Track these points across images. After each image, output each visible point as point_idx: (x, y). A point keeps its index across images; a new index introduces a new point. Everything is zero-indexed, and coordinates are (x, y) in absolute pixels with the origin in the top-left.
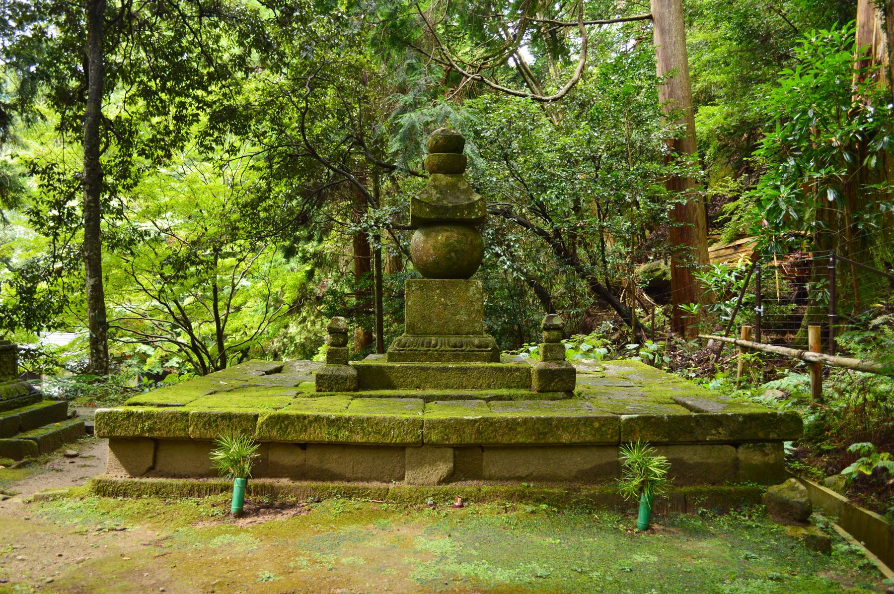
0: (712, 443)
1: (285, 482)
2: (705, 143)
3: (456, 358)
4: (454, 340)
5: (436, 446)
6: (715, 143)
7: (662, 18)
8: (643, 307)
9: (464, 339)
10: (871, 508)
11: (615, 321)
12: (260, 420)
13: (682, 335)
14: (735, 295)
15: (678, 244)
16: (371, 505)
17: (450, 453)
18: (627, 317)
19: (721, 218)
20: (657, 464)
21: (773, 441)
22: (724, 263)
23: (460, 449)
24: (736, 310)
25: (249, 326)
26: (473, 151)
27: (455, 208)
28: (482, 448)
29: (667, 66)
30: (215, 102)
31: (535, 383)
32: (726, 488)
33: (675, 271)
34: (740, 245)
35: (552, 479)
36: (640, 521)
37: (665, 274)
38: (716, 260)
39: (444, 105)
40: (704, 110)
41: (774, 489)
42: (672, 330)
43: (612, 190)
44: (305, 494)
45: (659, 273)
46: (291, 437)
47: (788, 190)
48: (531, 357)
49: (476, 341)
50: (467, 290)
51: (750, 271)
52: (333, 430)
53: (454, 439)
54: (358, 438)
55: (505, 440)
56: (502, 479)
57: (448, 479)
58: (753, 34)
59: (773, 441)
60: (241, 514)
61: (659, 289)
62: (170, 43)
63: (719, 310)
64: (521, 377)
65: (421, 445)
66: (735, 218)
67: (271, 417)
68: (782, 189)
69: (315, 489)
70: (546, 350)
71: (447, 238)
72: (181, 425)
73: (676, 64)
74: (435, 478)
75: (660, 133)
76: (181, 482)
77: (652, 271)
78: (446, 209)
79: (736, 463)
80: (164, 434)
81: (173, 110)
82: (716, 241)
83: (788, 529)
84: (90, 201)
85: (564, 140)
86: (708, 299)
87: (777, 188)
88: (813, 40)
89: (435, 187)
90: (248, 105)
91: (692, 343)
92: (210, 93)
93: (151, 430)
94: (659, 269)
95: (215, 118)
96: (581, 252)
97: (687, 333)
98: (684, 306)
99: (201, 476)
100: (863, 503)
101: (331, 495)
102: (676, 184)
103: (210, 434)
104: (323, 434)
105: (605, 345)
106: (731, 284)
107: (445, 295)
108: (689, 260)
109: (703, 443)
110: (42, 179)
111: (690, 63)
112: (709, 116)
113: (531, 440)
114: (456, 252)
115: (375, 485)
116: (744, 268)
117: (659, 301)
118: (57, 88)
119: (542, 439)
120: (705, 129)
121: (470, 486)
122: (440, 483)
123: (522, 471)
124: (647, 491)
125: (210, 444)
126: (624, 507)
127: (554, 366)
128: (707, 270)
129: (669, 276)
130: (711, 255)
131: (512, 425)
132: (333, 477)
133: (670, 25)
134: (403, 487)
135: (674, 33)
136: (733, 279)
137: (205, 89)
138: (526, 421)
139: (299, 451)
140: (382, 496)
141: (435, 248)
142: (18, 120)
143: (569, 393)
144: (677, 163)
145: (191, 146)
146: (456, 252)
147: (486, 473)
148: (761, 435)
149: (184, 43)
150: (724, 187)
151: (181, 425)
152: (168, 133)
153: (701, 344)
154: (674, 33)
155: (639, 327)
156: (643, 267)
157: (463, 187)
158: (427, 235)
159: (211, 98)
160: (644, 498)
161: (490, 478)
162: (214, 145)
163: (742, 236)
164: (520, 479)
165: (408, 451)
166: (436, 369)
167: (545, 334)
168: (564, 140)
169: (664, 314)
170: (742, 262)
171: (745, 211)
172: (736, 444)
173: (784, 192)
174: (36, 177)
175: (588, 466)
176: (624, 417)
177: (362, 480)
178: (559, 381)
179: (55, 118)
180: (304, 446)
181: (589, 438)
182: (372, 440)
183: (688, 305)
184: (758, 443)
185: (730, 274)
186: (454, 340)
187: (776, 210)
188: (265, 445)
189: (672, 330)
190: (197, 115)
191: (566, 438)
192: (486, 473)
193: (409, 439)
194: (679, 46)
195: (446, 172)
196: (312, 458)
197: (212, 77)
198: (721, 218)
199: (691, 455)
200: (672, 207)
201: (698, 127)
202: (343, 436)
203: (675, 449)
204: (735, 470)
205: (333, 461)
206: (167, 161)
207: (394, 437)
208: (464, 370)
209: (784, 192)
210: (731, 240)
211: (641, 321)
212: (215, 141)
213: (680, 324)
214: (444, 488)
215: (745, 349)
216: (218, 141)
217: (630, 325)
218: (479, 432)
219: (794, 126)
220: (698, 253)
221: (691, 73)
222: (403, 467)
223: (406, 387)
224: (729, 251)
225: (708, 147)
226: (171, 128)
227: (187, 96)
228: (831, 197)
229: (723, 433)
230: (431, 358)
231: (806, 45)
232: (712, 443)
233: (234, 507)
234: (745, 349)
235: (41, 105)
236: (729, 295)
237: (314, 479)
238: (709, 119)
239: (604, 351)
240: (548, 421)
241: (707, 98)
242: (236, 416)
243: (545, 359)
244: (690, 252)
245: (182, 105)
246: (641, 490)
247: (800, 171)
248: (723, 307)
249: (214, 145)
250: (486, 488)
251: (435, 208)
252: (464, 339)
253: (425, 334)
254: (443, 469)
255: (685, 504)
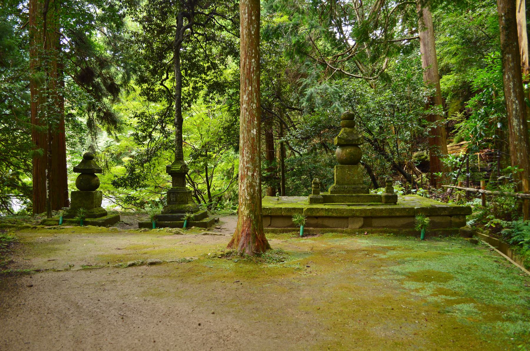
0: (443, 215)
1: (311, 228)
2: (446, 93)
3: (354, 192)
4: (353, 186)
5: (358, 217)
6: (451, 93)
7: (424, 39)
8: (416, 174)
9: (356, 186)
10: (496, 238)
11: (402, 181)
12: (304, 210)
13: (435, 187)
14: (458, 168)
15: (432, 145)
16: (339, 234)
17: (362, 219)
18: (409, 179)
19: (453, 131)
20: (427, 220)
21: (462, 215)
22: (454, 153)
23: (365, 218)
24: (459, 174)
25: (216, 185)
26: (339, 105)
27: (353, 140)
28: (372, 217)
29: (427, 64)
30: (210, 80)
31: (383, 200)
32: (447, 229)
33: (431, 157)
34: (462, 145)
35: (394, 227)
36: (422, 237)
37: (426, 157)
38: (451, 152)
39: (325, 84)
40: (445, 77)
41: (462, 228)
42: (430, 185)
43: (402, 121)
44: (318, 232)
45: (423, 157)
46: (314, 214)
47: (481, 123)
48: (381, 192)
49: (361, 187)
50: (357, 169)
51: (465, 158)
52: (327, 212)
53: (363, 215)
54: (335, 215)
55: (379, 215)
56: (378, 227)
57: (362, 227)
58: (469, 41)
59: (462, 215)
60: (303, 236)
61: (424, 166)
62: (190, 53)
63: (451, 175)
64: (378, 199)
65: (354, 216)
66: (460, 131)
67: (308, 209)
68: (478, 123)
69: (321, 230)
70: (387, 189)
71: (350, 151)
72: (280, 212)
73: (431, 60)
74: (358, 227)
75: (425, 93)
76: (280, 229)
77: (420, 156)
78: (350, 140)
79: (451, 222)
80: (275, 214)
81: (192, 85)
82: (451, 142)
83: (466, 239)
84: (179, 132)
85: (379, 98)
86: (447, 170)
87: (475, 122)
88: (492, 56)
89: (345, 133)
90: (226, 81)
91: (440, 190)
92: (207, 76)
93: (270, 213)
94: (423, 155)
95: (209, 87)
96: (387, 148)
97: (437, 186)
98: (436, 174)
99: (285, 227)
100: (494, 236)
101: (326, 232)
102: (432, 118)
103: (289, 214)
104: (323, 214)
105: (402, 190)
106: (456, 163)
107: (350, 171)
108: (438, 152)
109: (440, 215)
110: (139, 119)
111: (437, 53)
112: (448, 80)
113: (388, 215)
114: (353, 155)
115: (339, 229)
116: (463, 156)
117: (423, 171)
118: (140, 76)
119: (391, 215)
120: (446, 87)
121: (369, 229)
122: (359, 228)
123: (384, 225)
124: (423, 228)
125: (290, 217)
126: (416, 234)
127: (390, 194)
128: (446, 157)
129: (429, 158)
130: (448, 149)
131: (381, 210)
132: (326, 227)
133: (428, 42)
134: (349, 229)
135: (430, 46)
136: (458, 161)
137: (205, 74)
138: (385, 209)
139: (315, 219)
140: (342, 232)
141: (346, 154)
142: (123, 91)
143: (396, 204)
144: (432, 109)
145: (200, 100)
146: (353, 155)
147: (373, 225)
148: (458, 213)
149: (197, 53)
150: (455, 116)
151: (280, 212)
152: (189, 95)
153: (444, 191)
154: (430, 46)
155: (415, 183)
156: (415, 154)
157: (355, 132)
158: (343, 150)
159: (208, 78)
160: (423, 230)
161: (374, 227)
162: (210, 100)
163: (462, 140)
164: (384, 227)
165: (349, 219)
166: (349, 196)
167: (387, 184)
168: (379, 98)
169: (426, 177)
170: (462, 153)
171: (465, 127)
172: (451, 216)
173: (479, 124)
174: (136, 119)
175: (404, 223)
176: (416, 208)
177: (335, 227)
178: (392, 199)
179: (138, 89)
180: (317, 217)
181: (405, 214)
182: (339, 215)
183: (437, 173)
184: (458, 215)
185: (456, 159)
186: (353, 186)
187: (476, 130)
188: (308, 217)
189: (430, 185)
190: (203, 86)
191: (398, 214)
192: (373, 225)
193: (350, 215)
194: (432, 52)
195: (349, 127)
196: (320, 221)
197: (209, 68)
198: (453, 131)
199: (437, 219)
200: (430, 129)
201: (442, 86)
202: (330, 214)
203: (432, 217)
204: (450, 224)
205: (326, 222)
206: (189, 108)
207: (345, 214)
208: (358, 196)
209: (479, 124)
210: (459, 142)
211: (416, 180)
212: (211, 98)
213: (434, 182)
214: (361, 230)
215: (460, 190)
216: (213, 99)
217: (410, 182)
218: (371, 213)
219: (484, 94)
220: (443, 149)
221: (438, 58)
222: (348, 224)
223: (338, 202)
224: (457, 147)
225: (447, 95)
226: (191, 93)
227: (197, 77)
228: (499, 126)
229: (446, 213)
230: (346, 193)
231: (489, 58)
232: (443, 215)
233: (301, 234)
234: (460, 190)
235: (132, 83)
236: (455, 169)
237: (321, 227)
238: (448, 82)
239: (402, 192)
240: (392, 209)
241: (447, 70)
242: (297, 208)
243: (387, 192)
244: (438, 148)
245: (196, 82)
246: (421, 228)
247: (487, 114)
248: (453, 174)
249: (210, 100)
250: (374, 230)
251: (346, 140)
252: (356, 186)
253: (343, 184)
254: (360, 224)
255: (435, 234)
